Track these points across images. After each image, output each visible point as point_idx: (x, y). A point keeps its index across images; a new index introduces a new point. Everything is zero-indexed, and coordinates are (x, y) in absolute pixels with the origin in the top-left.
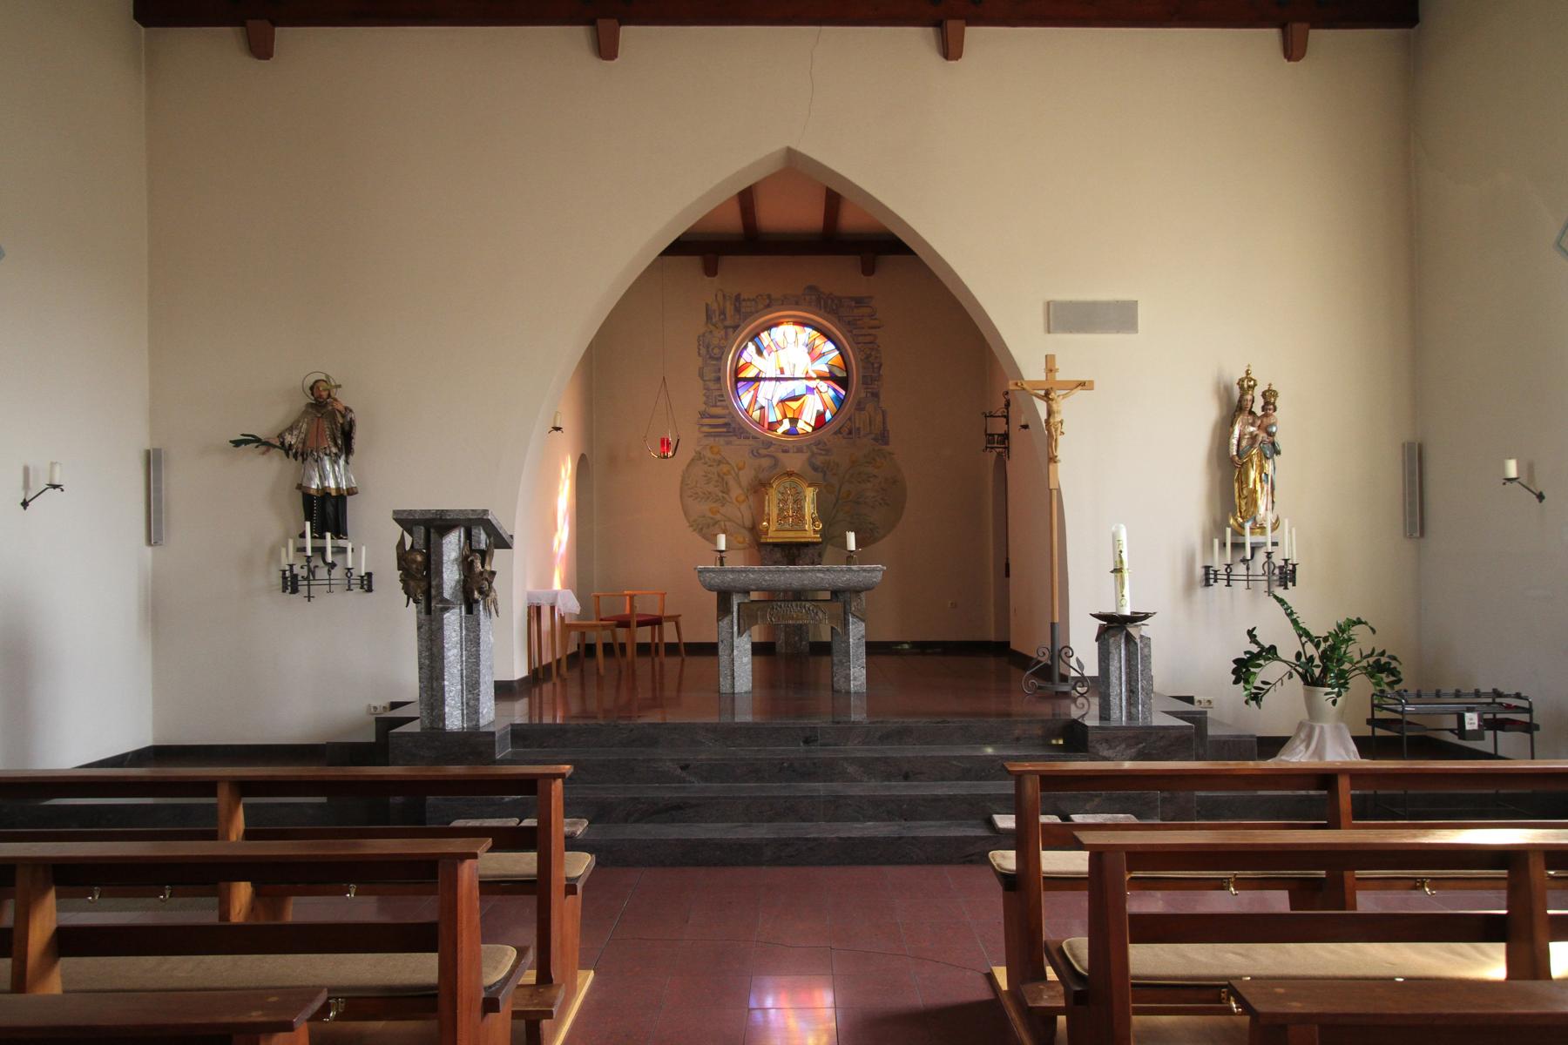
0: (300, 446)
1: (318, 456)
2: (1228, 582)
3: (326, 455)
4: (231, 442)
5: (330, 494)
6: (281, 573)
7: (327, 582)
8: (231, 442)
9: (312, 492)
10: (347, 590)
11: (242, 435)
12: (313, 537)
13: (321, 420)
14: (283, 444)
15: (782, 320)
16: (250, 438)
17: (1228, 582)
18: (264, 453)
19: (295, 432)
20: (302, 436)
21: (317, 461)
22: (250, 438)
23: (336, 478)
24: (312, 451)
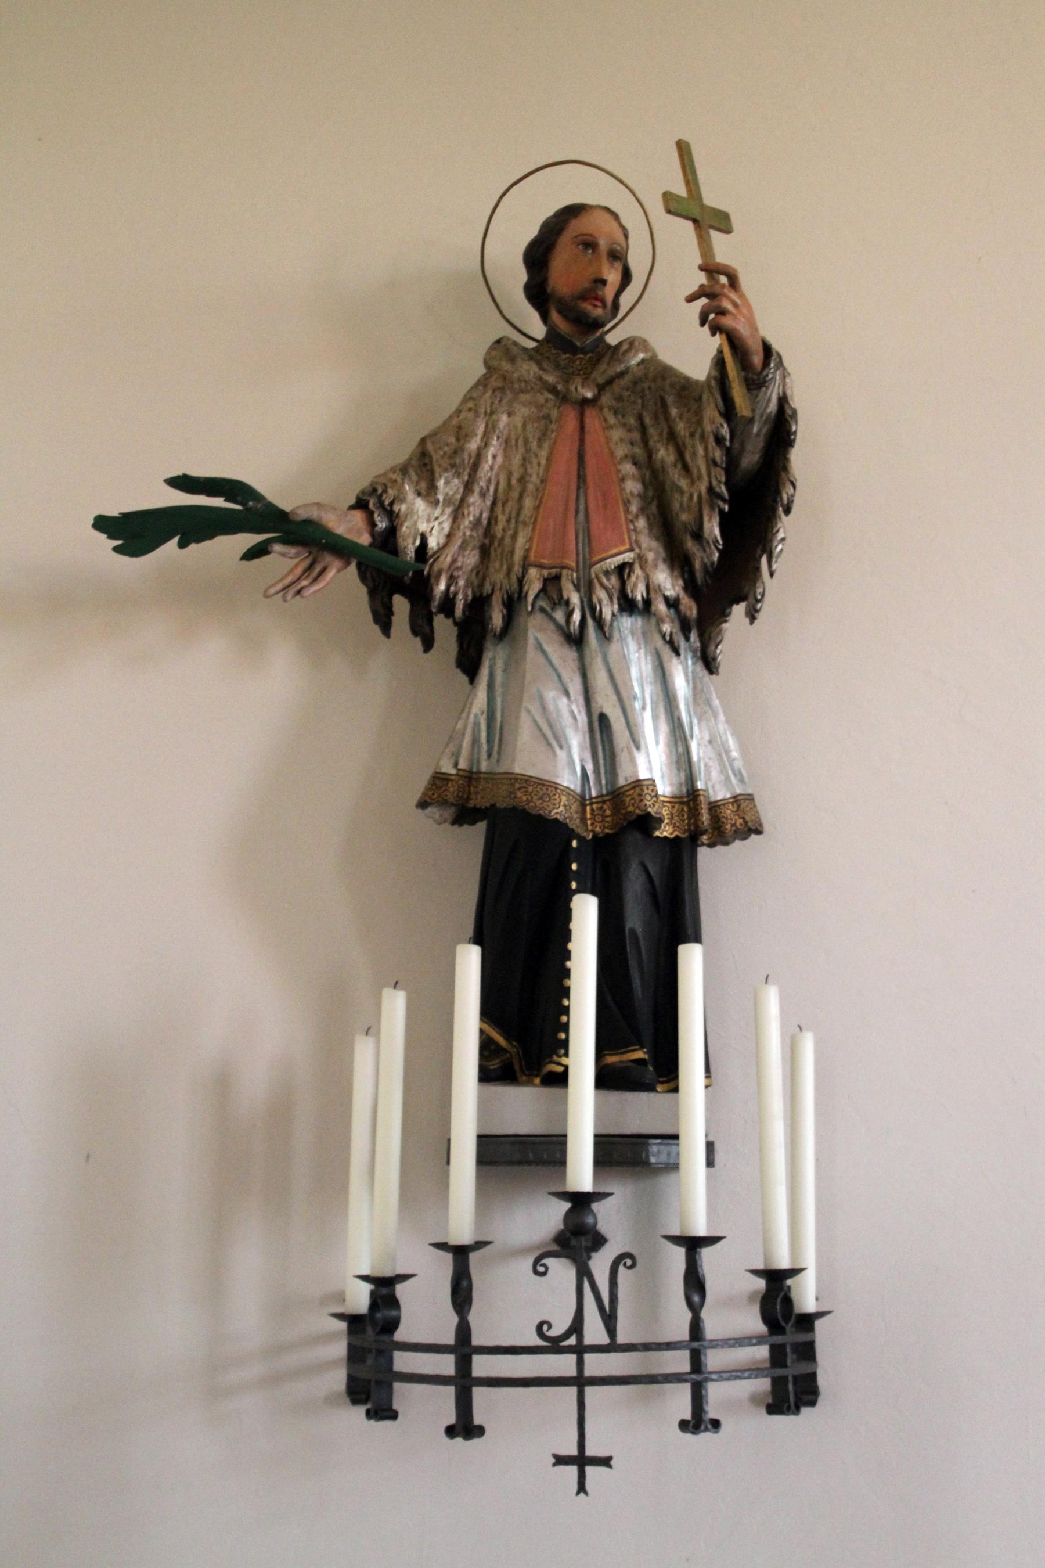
0: (471, 559)
1: (591, 609)
2: (464, 1404)
3: (628, 605)
4: (102, 524)
5: (646, 823)
6: (760, 1284)
7: (446, 1365)
8: (102, 524)
9: (560, 810)
10: (451, 1432)
11: (183, 483)
12: (605, 1079)
13: (590, 414)
14: (388, 541)
15: (476, 757)
16: (218, 502)
17: (464, 1404)
18: (293, 589)
19: (447, 486)
20: (477, 507)
21: (576, 641)
22: (218, 502)
23: (679, 735)
24: (552, 583)
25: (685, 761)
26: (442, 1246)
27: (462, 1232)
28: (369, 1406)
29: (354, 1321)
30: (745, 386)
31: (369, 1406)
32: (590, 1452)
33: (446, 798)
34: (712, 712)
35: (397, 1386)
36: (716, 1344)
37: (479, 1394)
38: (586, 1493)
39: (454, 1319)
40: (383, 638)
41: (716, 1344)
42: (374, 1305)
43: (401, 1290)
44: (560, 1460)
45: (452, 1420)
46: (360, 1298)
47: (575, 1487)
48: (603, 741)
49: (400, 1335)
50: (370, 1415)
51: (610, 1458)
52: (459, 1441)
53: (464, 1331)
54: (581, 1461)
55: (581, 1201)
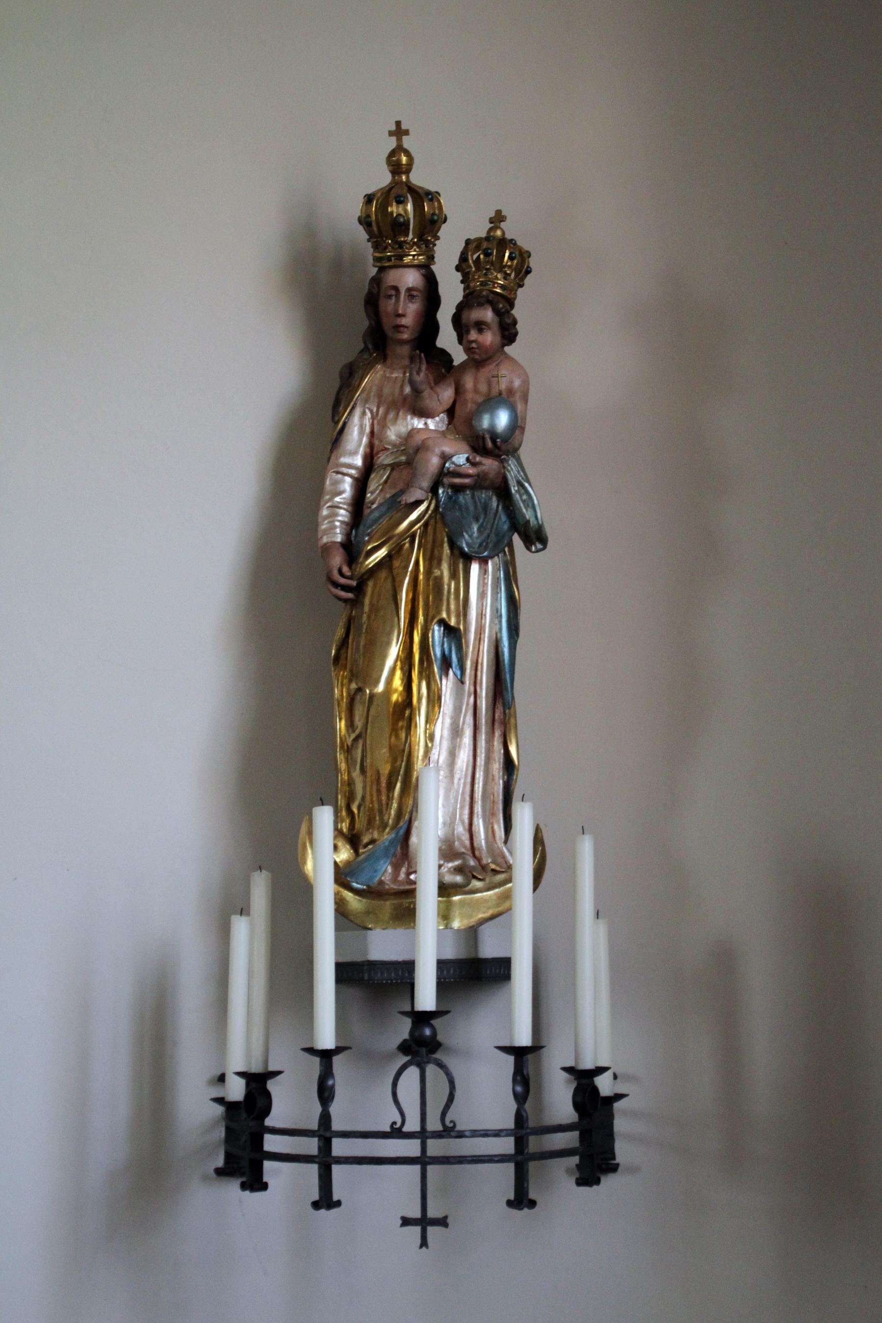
7: (311, 1146)
10: (316, 1205)
25: (463, 793)
26: (311, 1051)
27: (326, 1039)
28: (244, 1179)
29: (231, 1108)
30: (409, 853)
31: (244, 1179)
32: (417, 1229)
33: (389, 332)
34: (454, 831)
35: (268, 1165)
36: (502, 1159)
37: (337, 1171)
38: (446, 1217)
39: (318, 1109)
40: (210, 1098)
41: (502, 1159)
42: (249, 1095)
43: (272, 1086)
44: (406, 1222)
45: (316, 1197)
46: (236, 1090)
47: (419, 1241)
48: (435, 697)
49: (269, 1122)
50: (244, 1186)
51: (427, 1247)
52: (323, 1212)
53: (325, 1119)
54: (424, 1222)
55: (422, 1018)
